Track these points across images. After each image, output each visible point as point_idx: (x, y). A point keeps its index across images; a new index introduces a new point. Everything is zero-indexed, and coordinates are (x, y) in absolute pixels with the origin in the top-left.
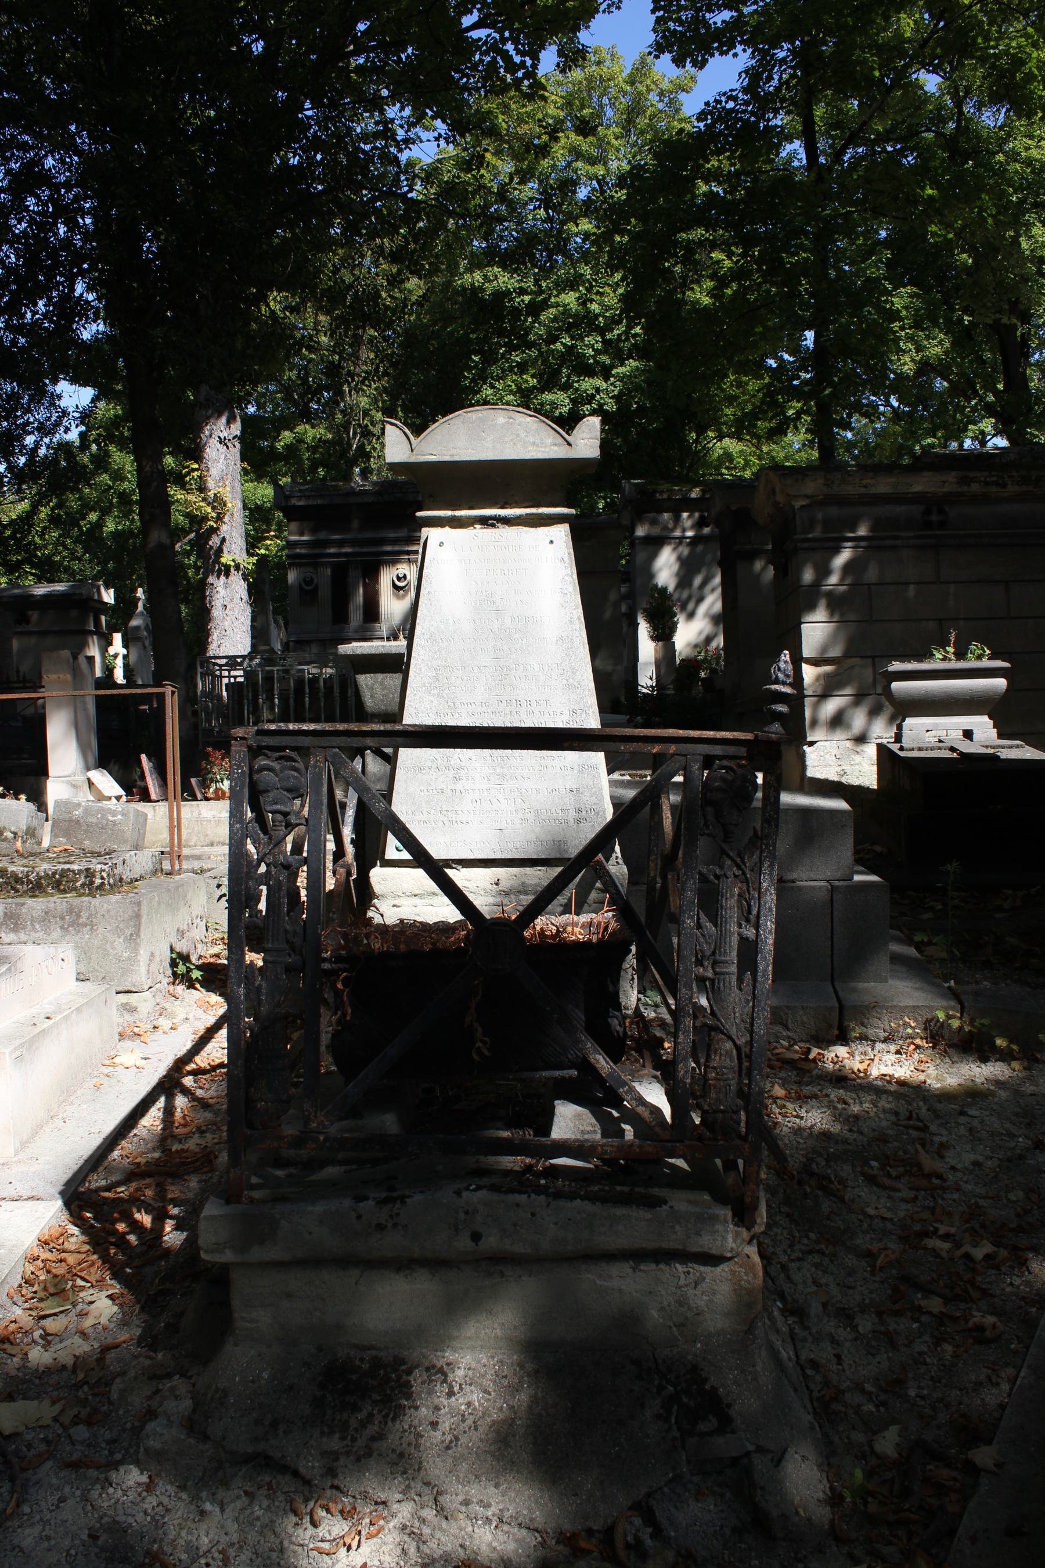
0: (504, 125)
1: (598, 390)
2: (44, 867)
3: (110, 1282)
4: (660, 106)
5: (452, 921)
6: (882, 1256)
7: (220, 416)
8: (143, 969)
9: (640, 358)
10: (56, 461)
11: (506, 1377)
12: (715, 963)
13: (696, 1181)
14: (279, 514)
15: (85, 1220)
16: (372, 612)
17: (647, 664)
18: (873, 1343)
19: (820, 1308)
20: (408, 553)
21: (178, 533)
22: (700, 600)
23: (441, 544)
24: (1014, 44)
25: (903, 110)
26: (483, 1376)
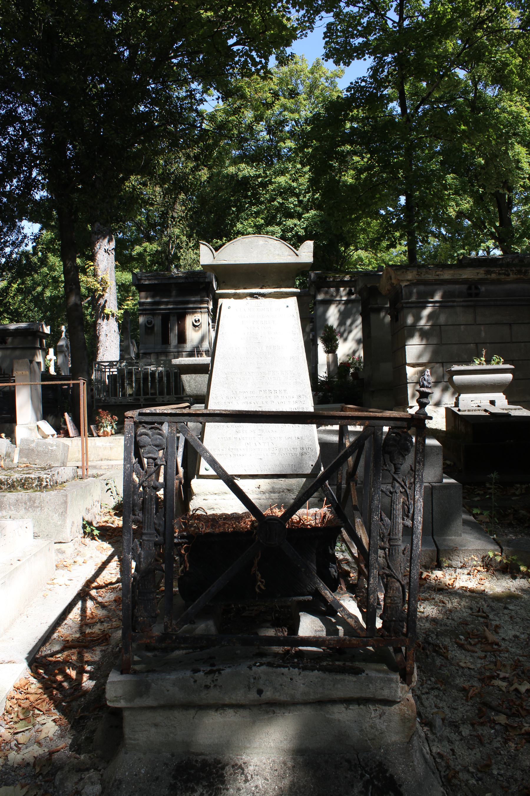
0: (249, 94)
1: (295, 225)
2: (16, 476)
3: (53, 711)
4: (326, 84)
5: (240, 513)
6: (471, 691)
7: (105, 238)
8: (68, 530)
9: (316, 210)
10: (20, 260)
11: (276, 770)
12: (390, 540)
13: (380, 657)
14: (133, 288)
15: (39, 674)
16: (182, 338)
17: (323, 365)
18: (471, 742)
19: (441, 722)
20: (200, 308)
21: (82, 297)
22: (350, 332)
23: (229, 308)
24: (504, 56)
25: (449, 87)
26: (264, 770)
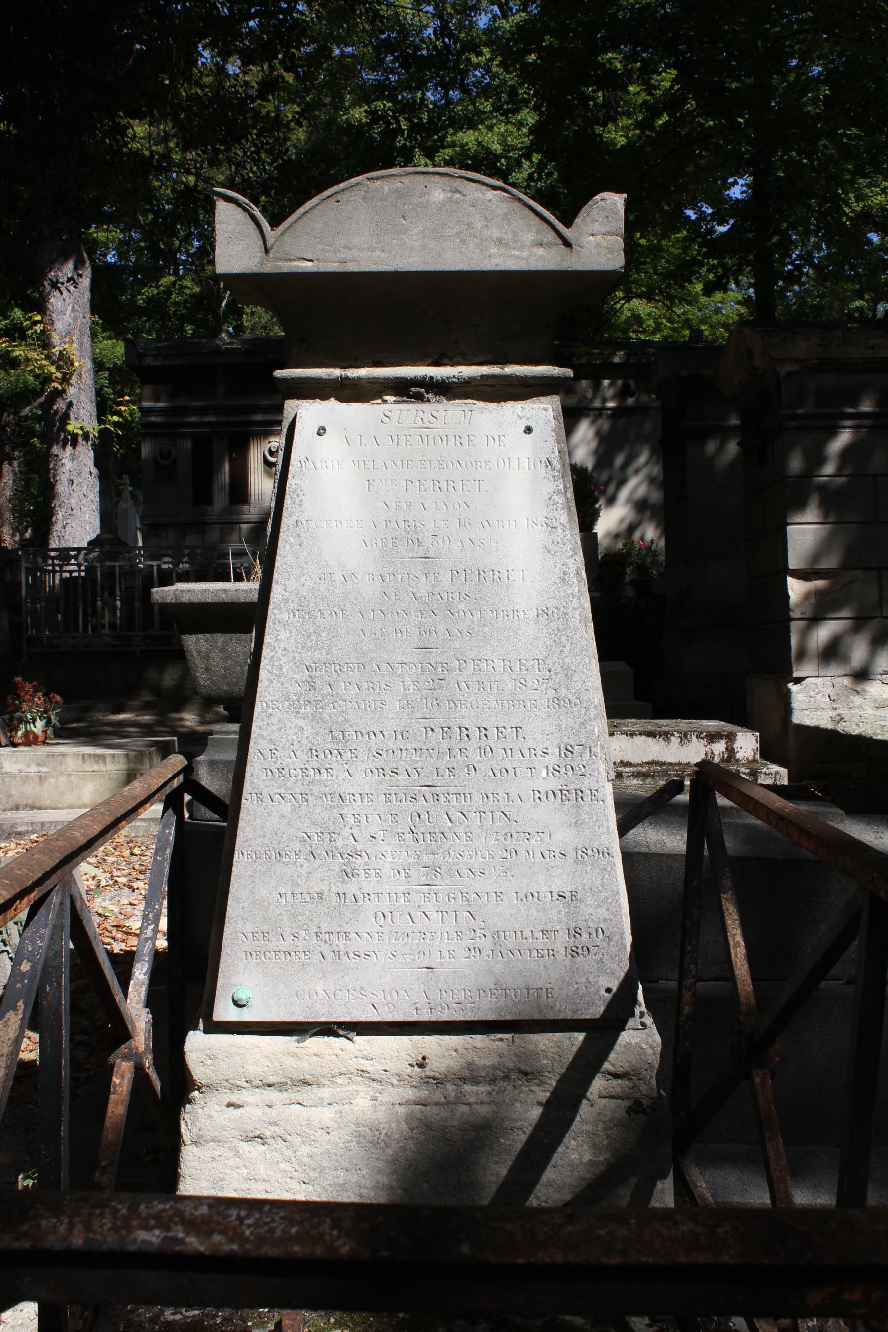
7: (66, 260)
22: (622, 482)
23: (321, 431)
